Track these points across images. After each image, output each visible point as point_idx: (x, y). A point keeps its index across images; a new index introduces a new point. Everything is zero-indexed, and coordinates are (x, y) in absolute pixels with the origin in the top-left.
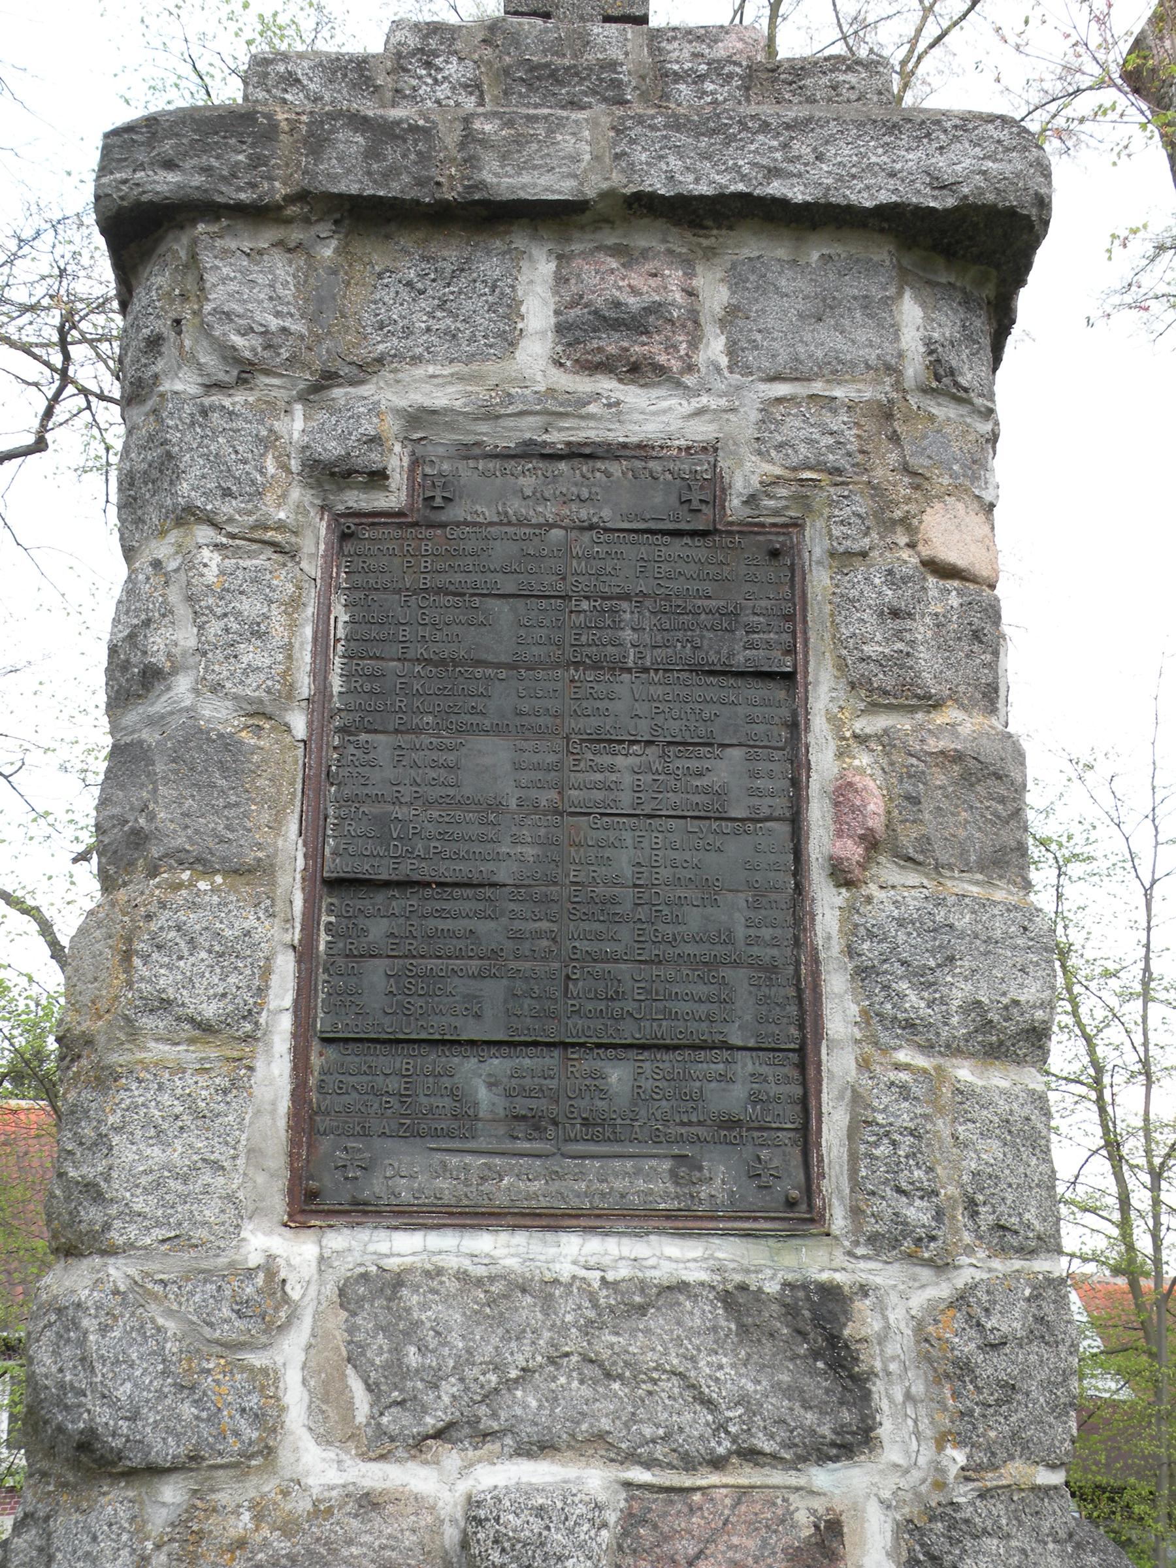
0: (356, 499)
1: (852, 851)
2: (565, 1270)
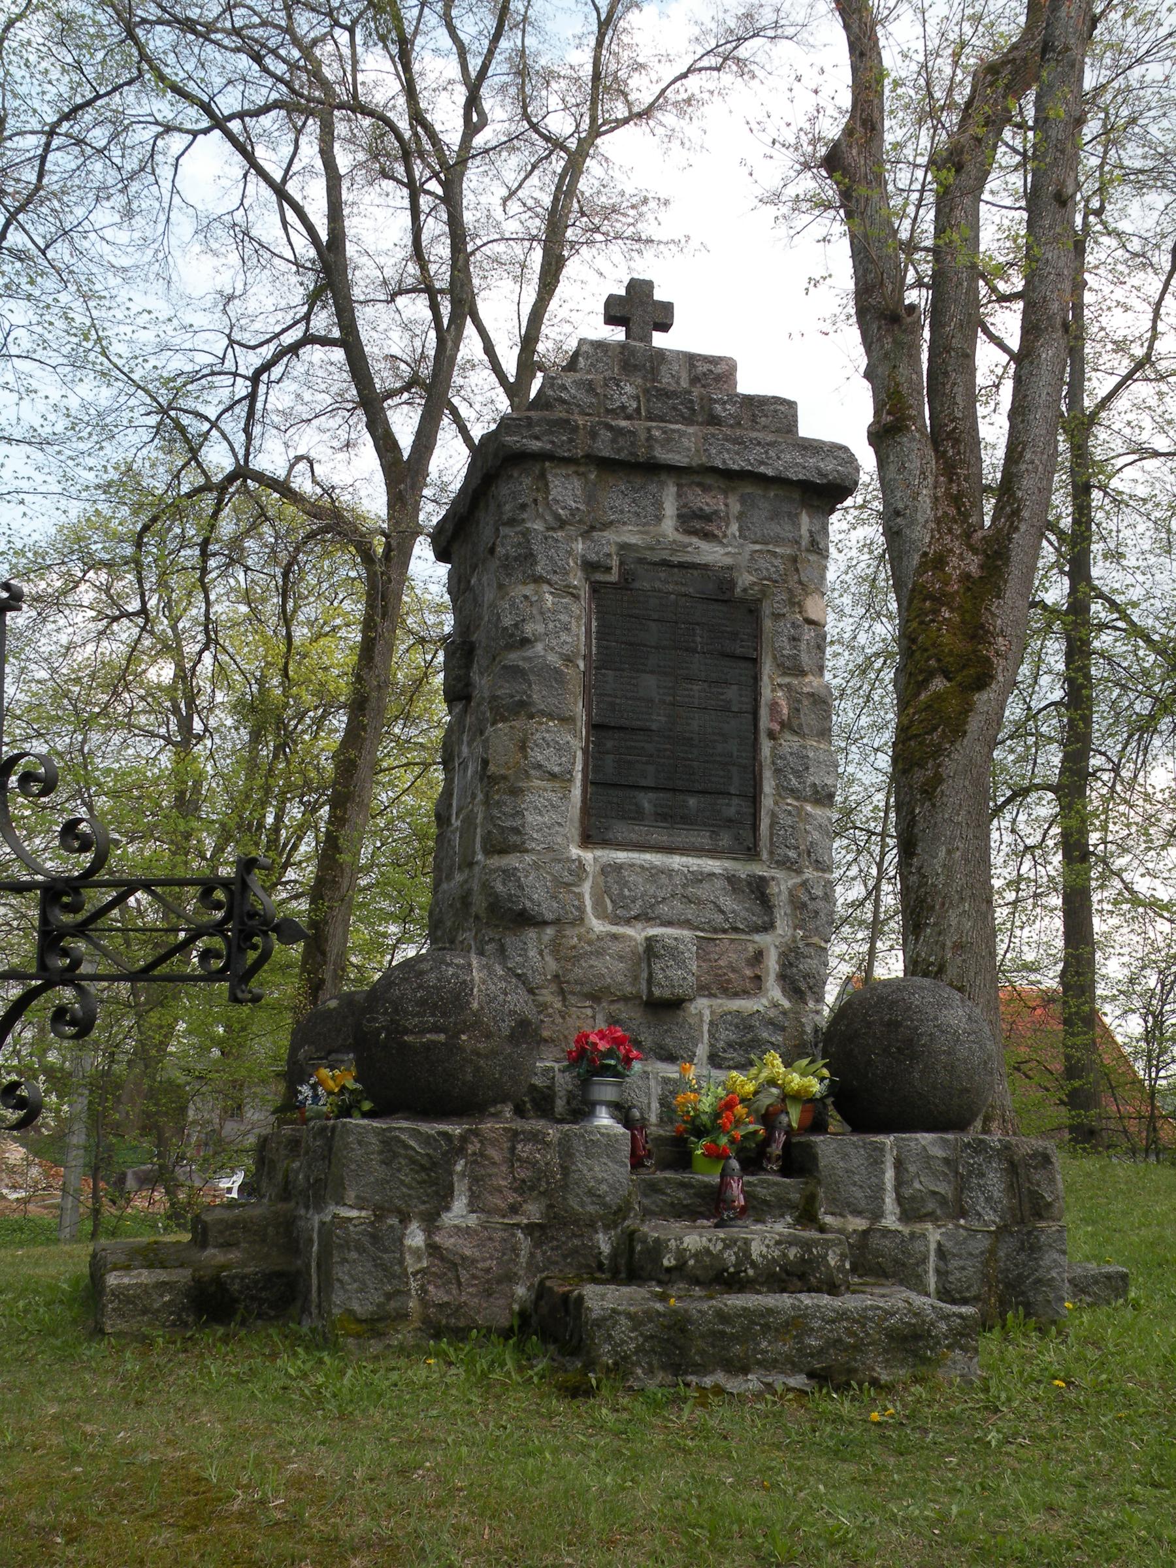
0: (600, 577)
1: (777, 727)
2: (676, 867)
